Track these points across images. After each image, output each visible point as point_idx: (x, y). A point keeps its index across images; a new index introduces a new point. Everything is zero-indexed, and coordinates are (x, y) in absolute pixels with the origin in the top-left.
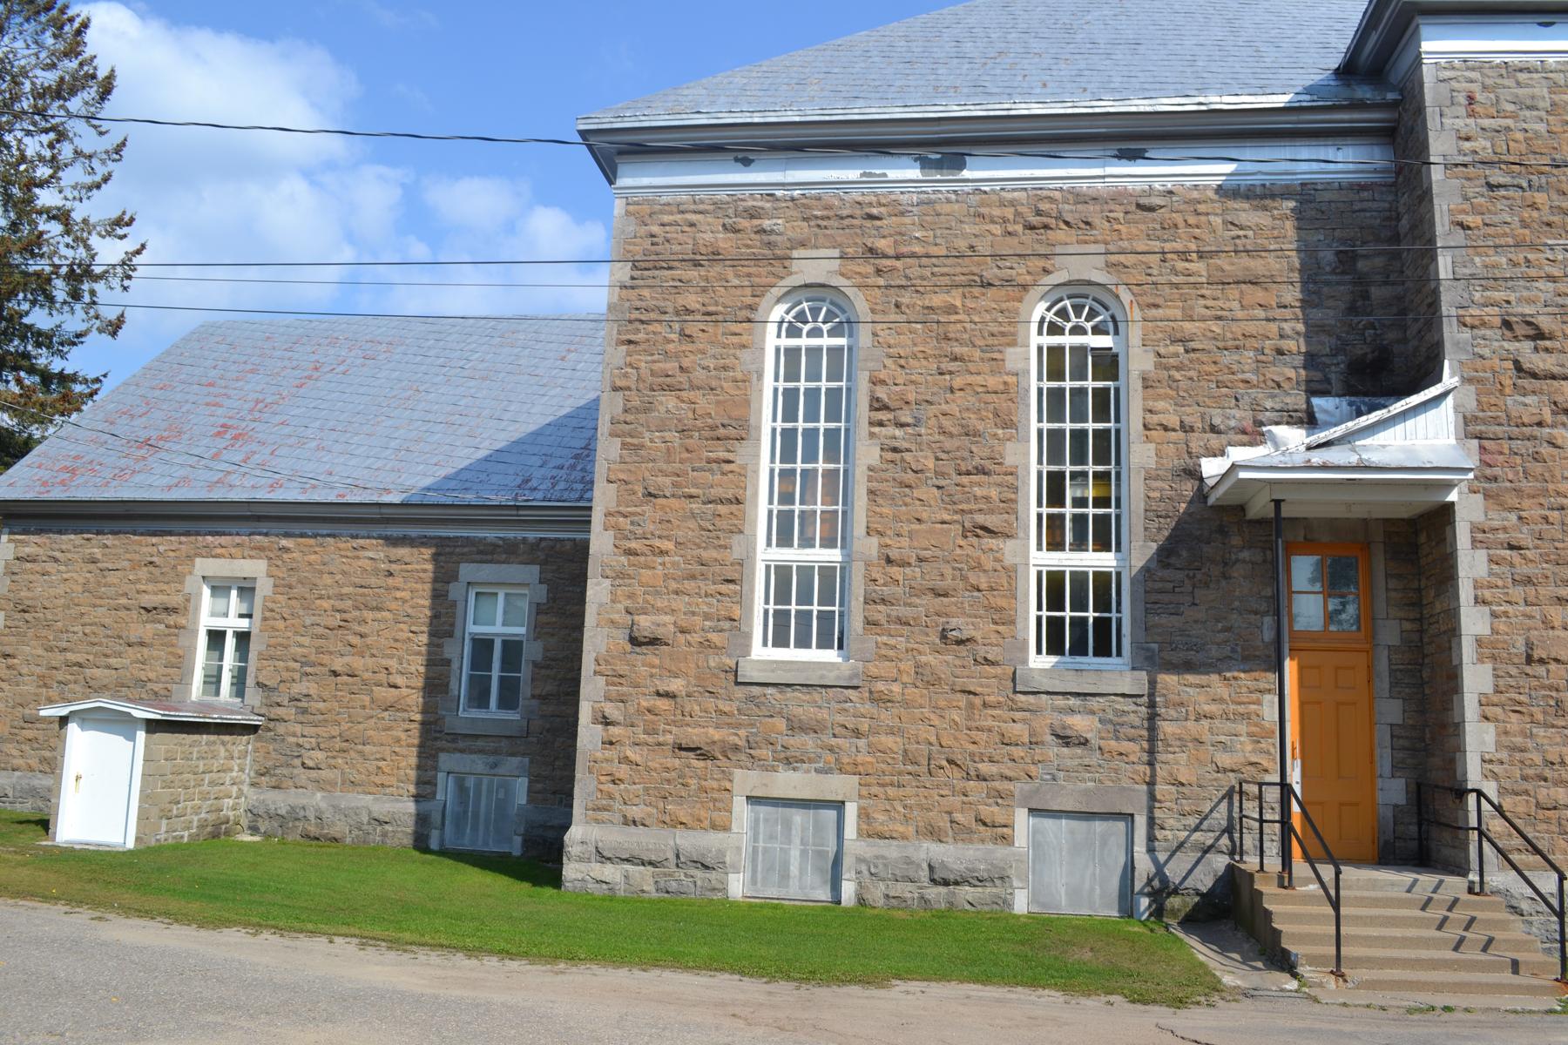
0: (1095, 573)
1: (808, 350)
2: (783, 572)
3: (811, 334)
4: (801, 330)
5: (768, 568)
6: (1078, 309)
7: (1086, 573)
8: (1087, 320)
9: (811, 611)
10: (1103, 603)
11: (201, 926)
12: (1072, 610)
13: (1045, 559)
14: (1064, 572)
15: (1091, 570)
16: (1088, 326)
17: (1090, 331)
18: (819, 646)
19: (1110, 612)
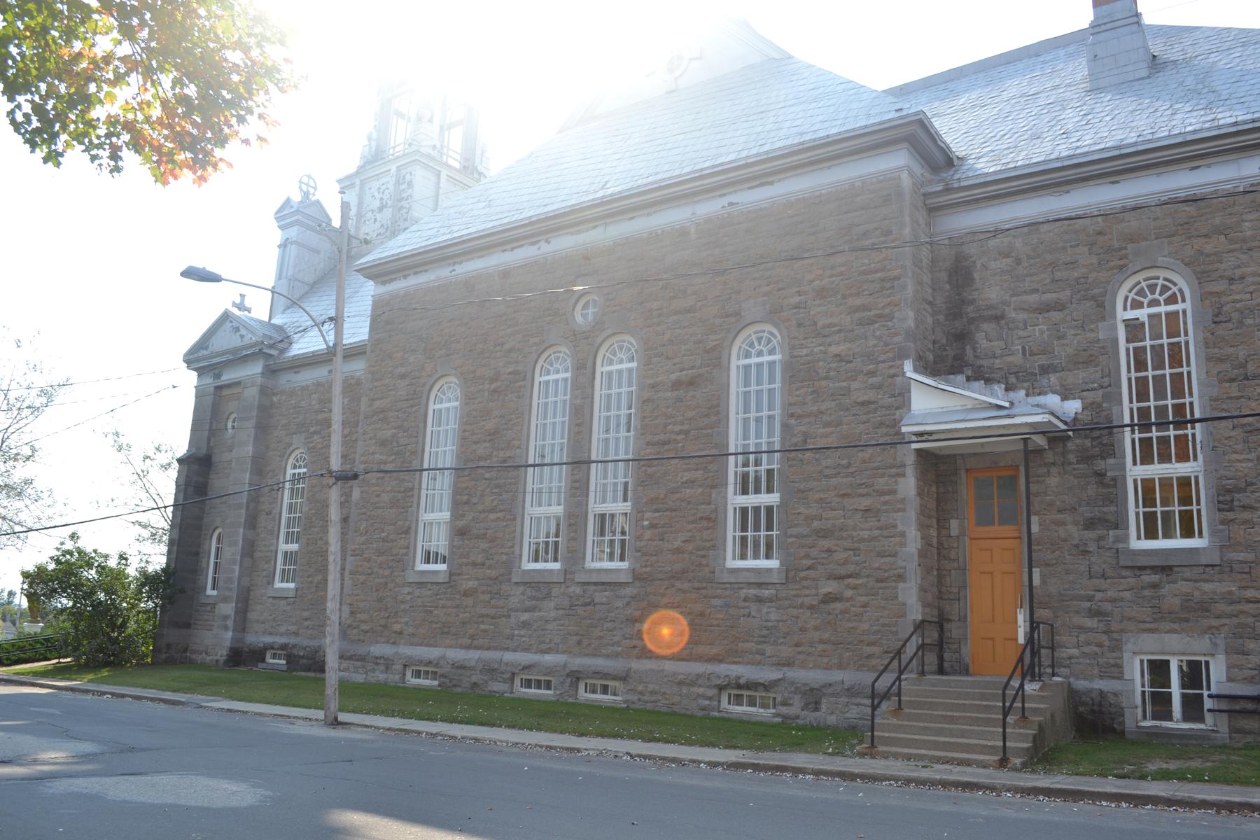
0: (1159, 479)
1: (1167, 314)
2: (1148, 485)
3: (1150, 305)
4: (1143, 303)
5: (735, 509)
6: (759, 340)
7: (1154, 479)
8: (1160, 295)
9: (1155, 513)
10: (1185, 500)
11: (702, 746)
12: (1162, 506)
13: (1136, 472)
14: (1154, 479)
15: (1156, 477)
16: (1161, 299)
17: (1162, 302)
18: (1183, 536)
19: (1156, 507)
